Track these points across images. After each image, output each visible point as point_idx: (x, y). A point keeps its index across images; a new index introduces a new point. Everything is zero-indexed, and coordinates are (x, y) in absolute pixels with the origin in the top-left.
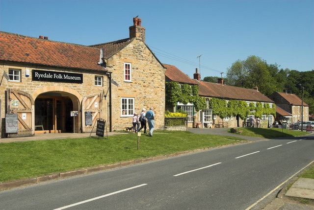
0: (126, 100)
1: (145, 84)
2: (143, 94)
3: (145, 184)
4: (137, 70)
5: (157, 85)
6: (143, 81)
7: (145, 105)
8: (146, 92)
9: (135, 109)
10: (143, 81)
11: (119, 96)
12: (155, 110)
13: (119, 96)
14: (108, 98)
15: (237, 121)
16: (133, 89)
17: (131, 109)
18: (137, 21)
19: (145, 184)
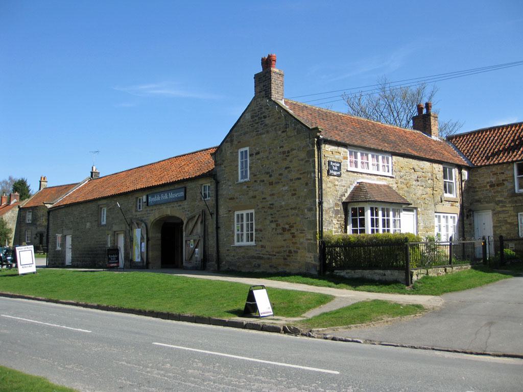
0: (242, 215)
1: (273, 179)
2: (269, 198)
3: (154, 343)
4: (258, 156)
5: (294, 175)
6: (268, 173)
7: (272, 222)
8: (273, 195)
9: (256, 230)
10: (268, 173)
11: (230, 211)
12: (293, 230)
13: (230, 211)
14: (215, 216)
15: (502, 354)
16: (251, 194)
17: (386, 218)
18: (267, 63)
19: (154, 343)
